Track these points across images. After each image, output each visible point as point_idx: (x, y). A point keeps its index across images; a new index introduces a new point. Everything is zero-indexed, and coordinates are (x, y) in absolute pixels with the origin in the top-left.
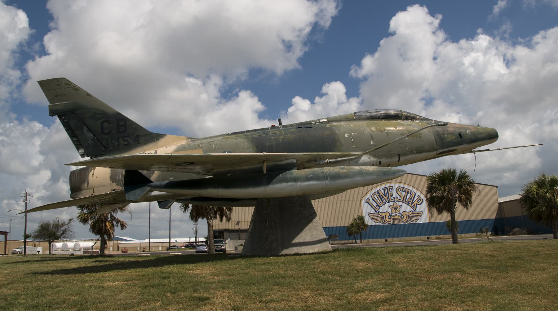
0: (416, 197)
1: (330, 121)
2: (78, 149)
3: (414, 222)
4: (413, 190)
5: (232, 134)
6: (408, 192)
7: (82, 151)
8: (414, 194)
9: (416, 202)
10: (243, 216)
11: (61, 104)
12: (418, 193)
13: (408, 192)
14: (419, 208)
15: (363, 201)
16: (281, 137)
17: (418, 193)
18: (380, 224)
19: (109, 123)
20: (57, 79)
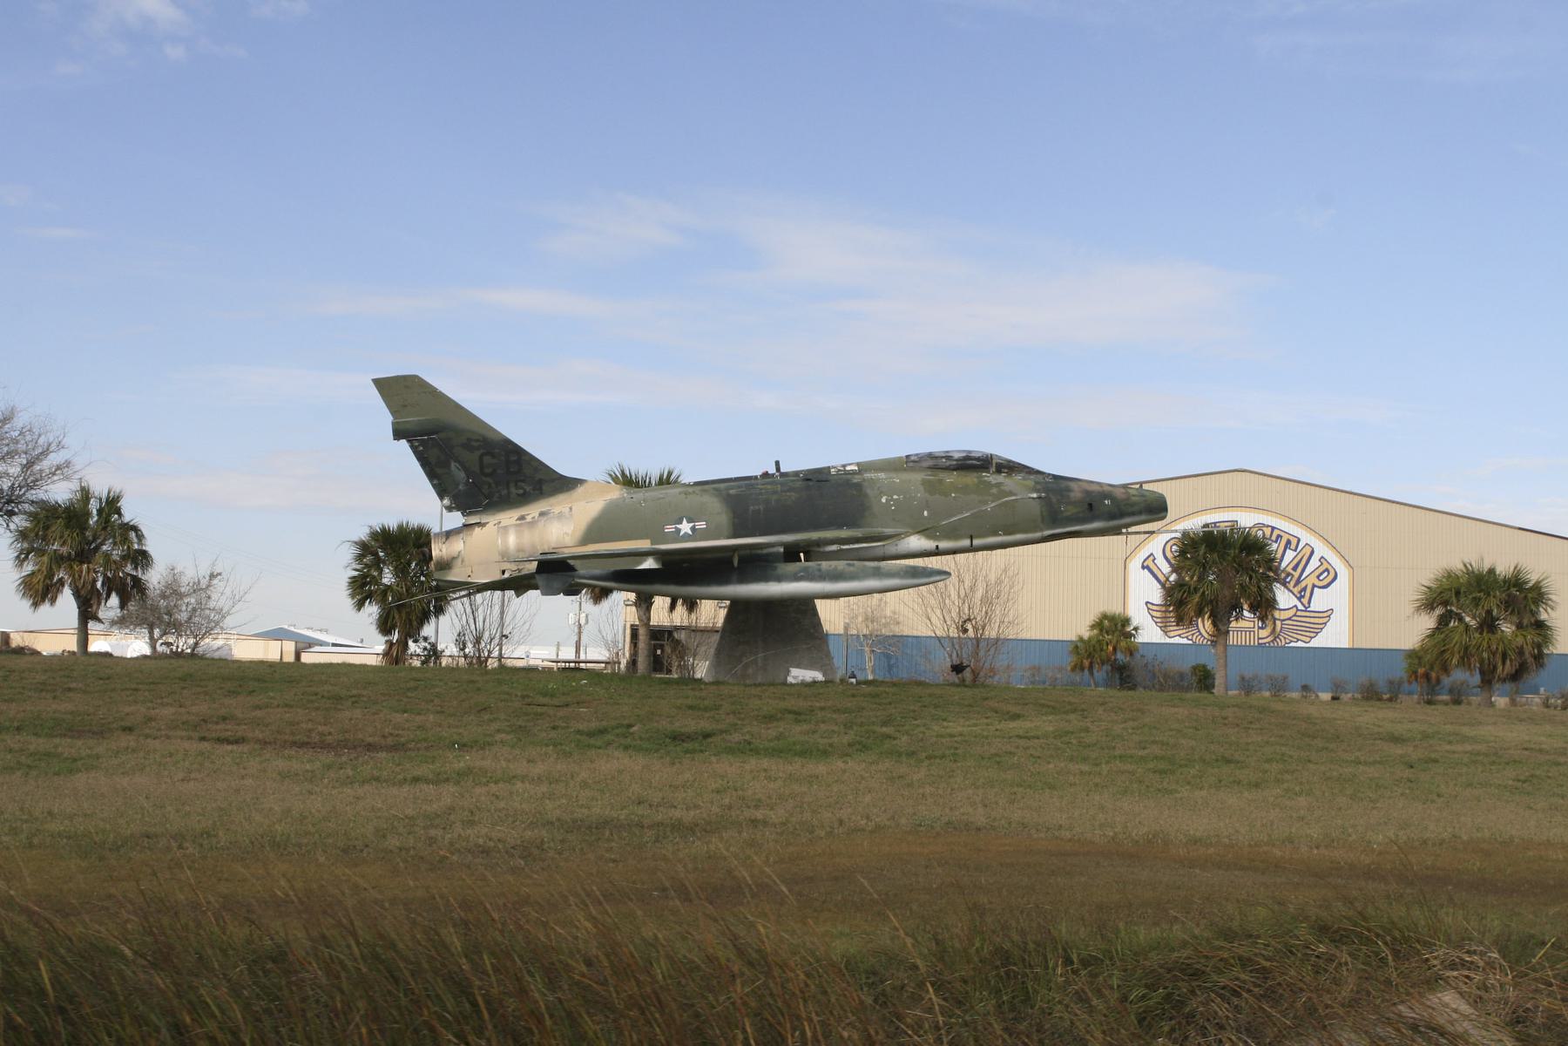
0: (1314, 563)
1: (864, 467)
2: (441, 498)
3: (1300, 644)
4: (1306, 537)
5: (697, 484)
6: (1289, 542)
7: (446, 501)
8: (1307, 551)
9: (1313, 580)
10: (712, 613)
11: (412, 419)
12: (1321, 550)
13: (1289, 542)
14: (1320, 600)
15: (1135, 564)
16: (775, 497)
17: (1321, 550)
18: (1185, 641)
19: (493, 456)
20: (405, 377)
